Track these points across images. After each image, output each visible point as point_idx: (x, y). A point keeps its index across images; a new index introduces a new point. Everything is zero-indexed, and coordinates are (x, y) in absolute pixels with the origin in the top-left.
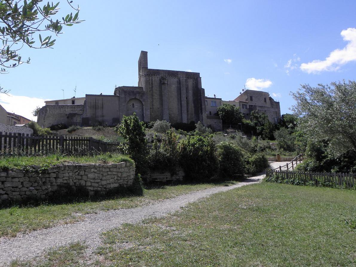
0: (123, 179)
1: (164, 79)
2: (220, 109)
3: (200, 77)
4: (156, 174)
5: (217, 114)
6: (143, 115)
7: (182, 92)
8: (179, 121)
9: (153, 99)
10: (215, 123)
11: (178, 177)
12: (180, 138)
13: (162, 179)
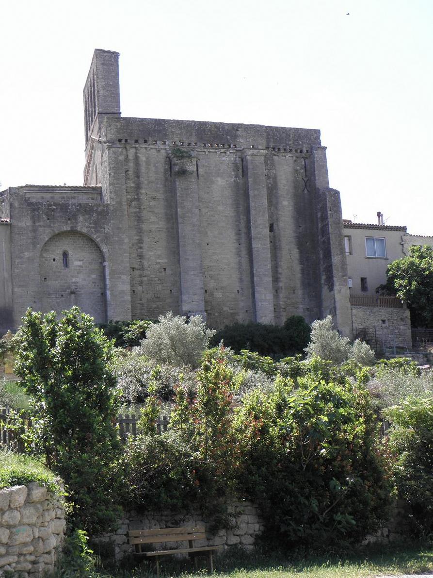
0: (16, 550)
1: (183, 157)
2: (398, 268)
3: (323, 144)
4: (150, 528)
5: (388, 288)
6: (104, 294)
7: (252, 204)
8: (242, 318)
9: (140, 231)
10: (384, 321)
11: (234, 540)
12: (245, 385)
13: (171, 549)
